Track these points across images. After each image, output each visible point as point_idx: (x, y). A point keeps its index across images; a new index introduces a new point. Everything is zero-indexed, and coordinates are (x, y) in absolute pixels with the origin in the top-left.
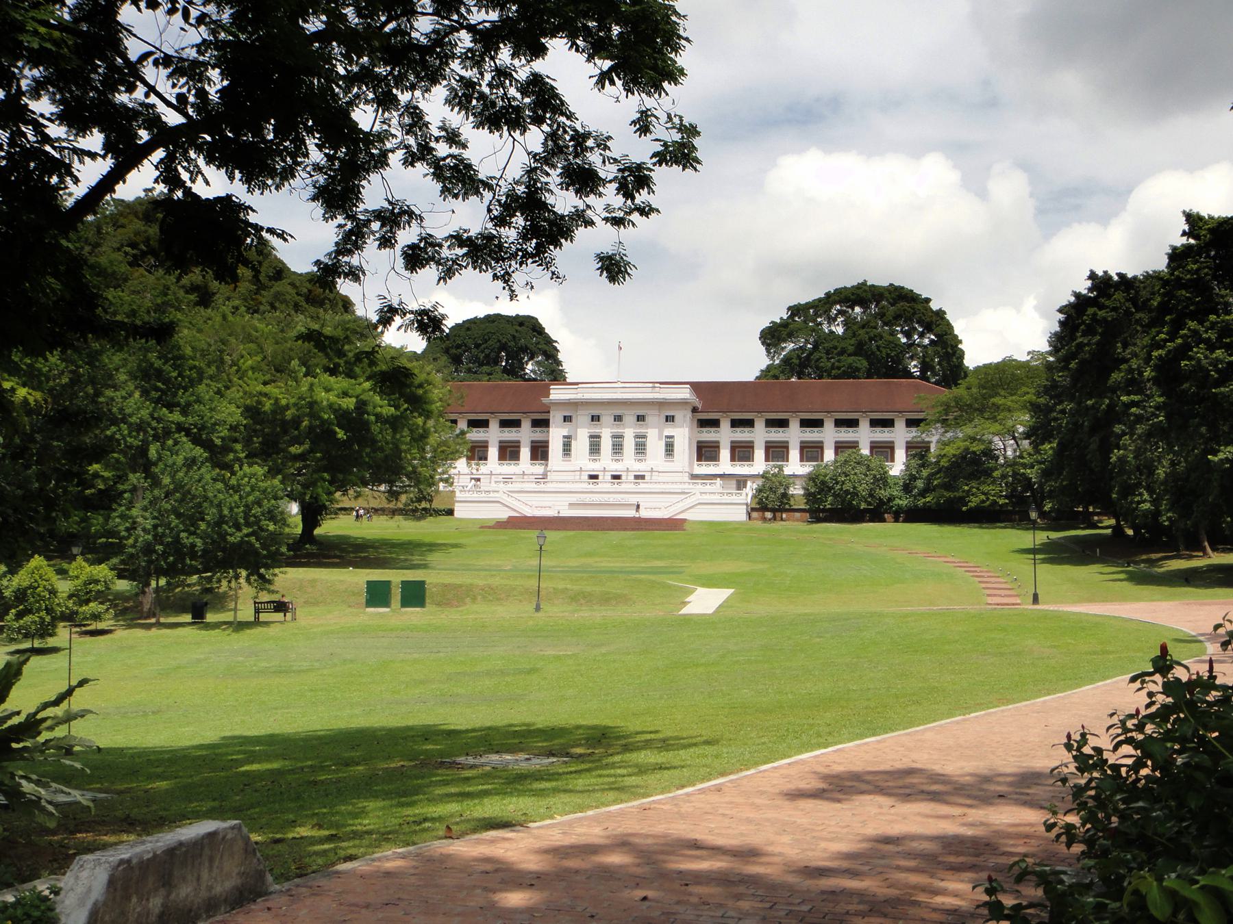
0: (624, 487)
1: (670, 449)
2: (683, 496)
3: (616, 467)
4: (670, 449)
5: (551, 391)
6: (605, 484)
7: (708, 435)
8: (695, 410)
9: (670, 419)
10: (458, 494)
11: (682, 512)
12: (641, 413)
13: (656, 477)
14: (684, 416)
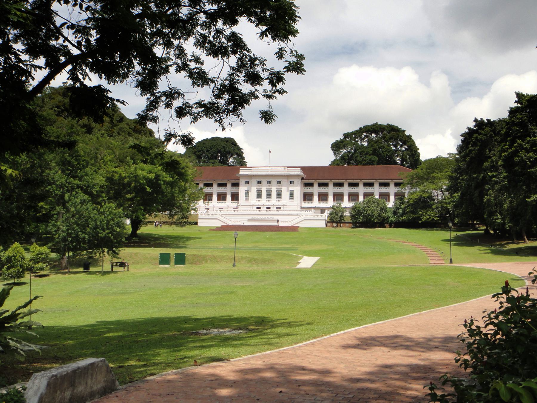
0: (272, 212)
1: (292, 196)
2: (298, 216)
3: (268, 204)
4: (292, 196)
5: (240, 171)
6: (263, 211)
7: (309, 190)
8: (303, 179)
9: (292, 183)
10: (199, 215)
11: (297, 223)
12: (279, 180)
13: (286, 208)
14: (298, 182)
